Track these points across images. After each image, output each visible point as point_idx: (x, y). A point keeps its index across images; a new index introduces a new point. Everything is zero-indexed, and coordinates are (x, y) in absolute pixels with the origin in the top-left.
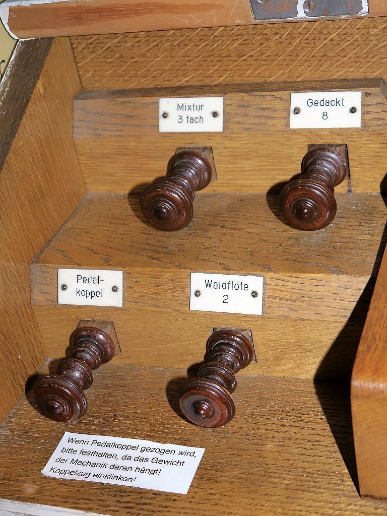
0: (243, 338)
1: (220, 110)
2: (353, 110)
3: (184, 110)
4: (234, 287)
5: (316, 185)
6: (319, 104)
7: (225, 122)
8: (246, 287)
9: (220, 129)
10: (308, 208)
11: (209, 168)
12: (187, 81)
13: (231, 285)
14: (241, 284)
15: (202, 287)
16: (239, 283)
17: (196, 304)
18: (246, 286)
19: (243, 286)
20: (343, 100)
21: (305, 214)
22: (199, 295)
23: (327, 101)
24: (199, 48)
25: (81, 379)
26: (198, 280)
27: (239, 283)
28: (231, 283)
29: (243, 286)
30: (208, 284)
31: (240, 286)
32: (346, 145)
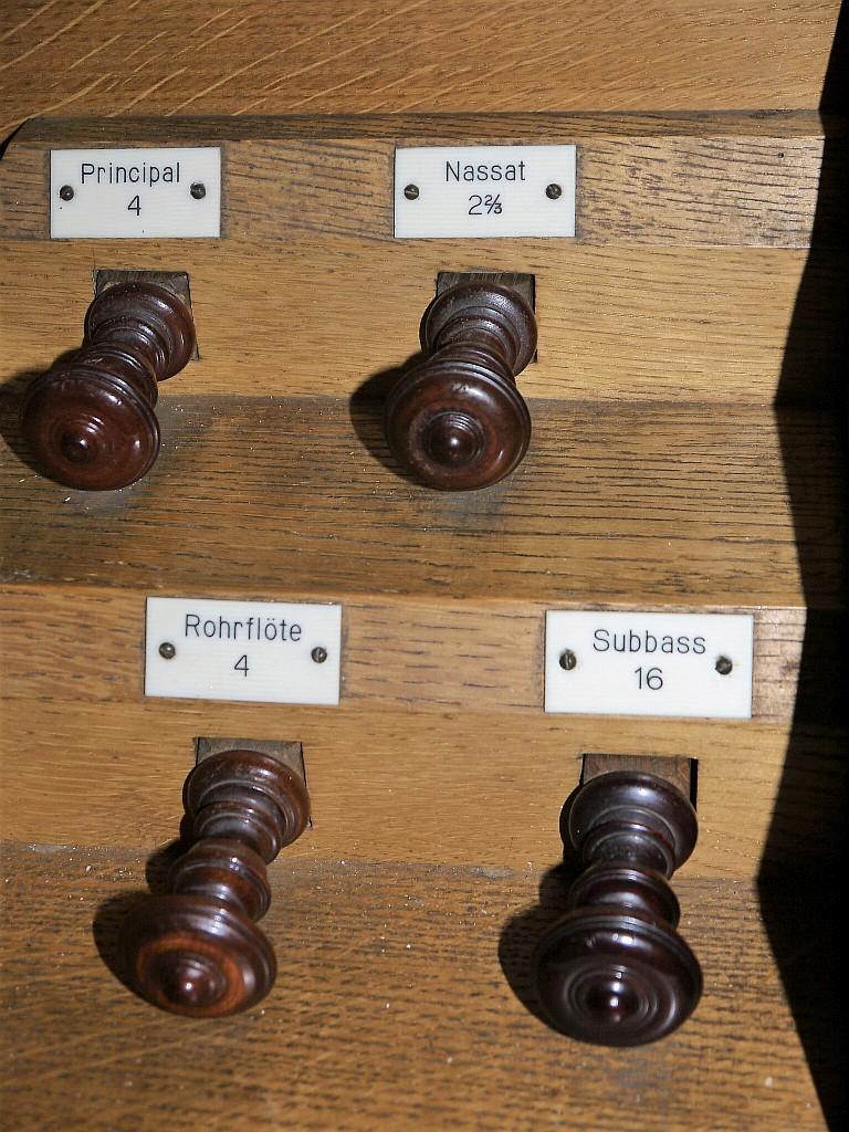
0: (281, 771)
1: (211, 177)
2: (553, 192)
3: (114, 180)
4: (262, 633)
5: (478, 372)
6: (162, 173)
7: (579, 212)
8: (295, 632)
9: (568, 230)
10: (88, 436)
11: (182, 321)
12: (575, 102)
13: (254, 628)
14: (283, 625)
15: (173, 632)
16: (278, 623)
17: (162, 680)
18: (295, 629)
19: (287, 629)
20: (522, 166)
21: (454, 449)
22: (173, 651)
23: (468, 169)
24: (385, 19)
25: (243, 871)
26: (165, 615)
27: (278, 623)
28: (255, 621)
29: (287, 629)
30: (192, 623)
31: (279, 629)
32: (533, 277)
